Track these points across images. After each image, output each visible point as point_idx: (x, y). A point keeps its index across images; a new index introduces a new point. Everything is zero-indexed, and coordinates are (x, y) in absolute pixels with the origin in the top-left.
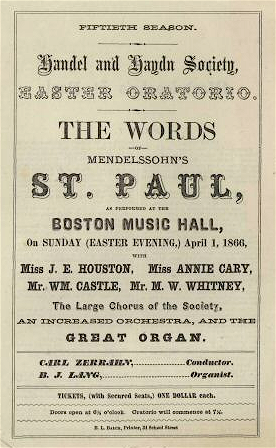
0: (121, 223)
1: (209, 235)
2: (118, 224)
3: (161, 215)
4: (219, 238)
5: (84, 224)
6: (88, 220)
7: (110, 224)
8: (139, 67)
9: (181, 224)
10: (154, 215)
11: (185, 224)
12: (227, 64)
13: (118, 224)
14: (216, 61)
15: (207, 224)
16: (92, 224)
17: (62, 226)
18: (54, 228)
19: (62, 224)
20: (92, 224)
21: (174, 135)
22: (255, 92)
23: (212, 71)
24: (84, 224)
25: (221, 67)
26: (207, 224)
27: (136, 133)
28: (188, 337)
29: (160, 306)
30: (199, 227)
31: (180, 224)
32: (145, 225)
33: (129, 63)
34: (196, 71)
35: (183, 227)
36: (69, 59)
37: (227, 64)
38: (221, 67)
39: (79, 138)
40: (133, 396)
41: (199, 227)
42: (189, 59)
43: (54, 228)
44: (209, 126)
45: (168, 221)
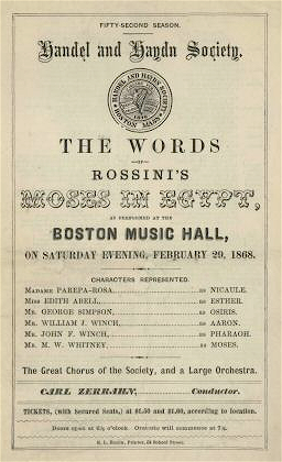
0: (124, 232)
1: (209, 246)
2: (121, 234)
3: (165, 225)
4: (226, 248)
5: (85, 234)
6: (90, 230)
7: (112, 234)
8: (49, 53)
9: (186, 234)
10: (158, 224)
11: (190, 233)
12: (231, 50)
13: (121, 234)
14: (221, 46)
15: (212, 234)
16: (94, 234)
17: (63, 236)
18: (55, 238)
19: (63, 234)
20: (94, 234)
21: (178, 149)
22: (20, 257)
23: (216, 57)
24: (85, 234)
25: (226, 53)
26: (212, 234)
27: (137, 148)
28: (133, 411)
29: (107, 371)
30: (204, 235)
31: (184, 233)
32: (149, 234)
33: (131, 49)
34: (200, 56)
35: (187, 237)
36: (161, 45)
37: (231, 50)
38: (226, 53)
39: (89, 141)
40: (101, 412)
41: (204, 235)
42: (192, 45)
43: (55, 238)
44: (215, 143)
45: (172, 231)
